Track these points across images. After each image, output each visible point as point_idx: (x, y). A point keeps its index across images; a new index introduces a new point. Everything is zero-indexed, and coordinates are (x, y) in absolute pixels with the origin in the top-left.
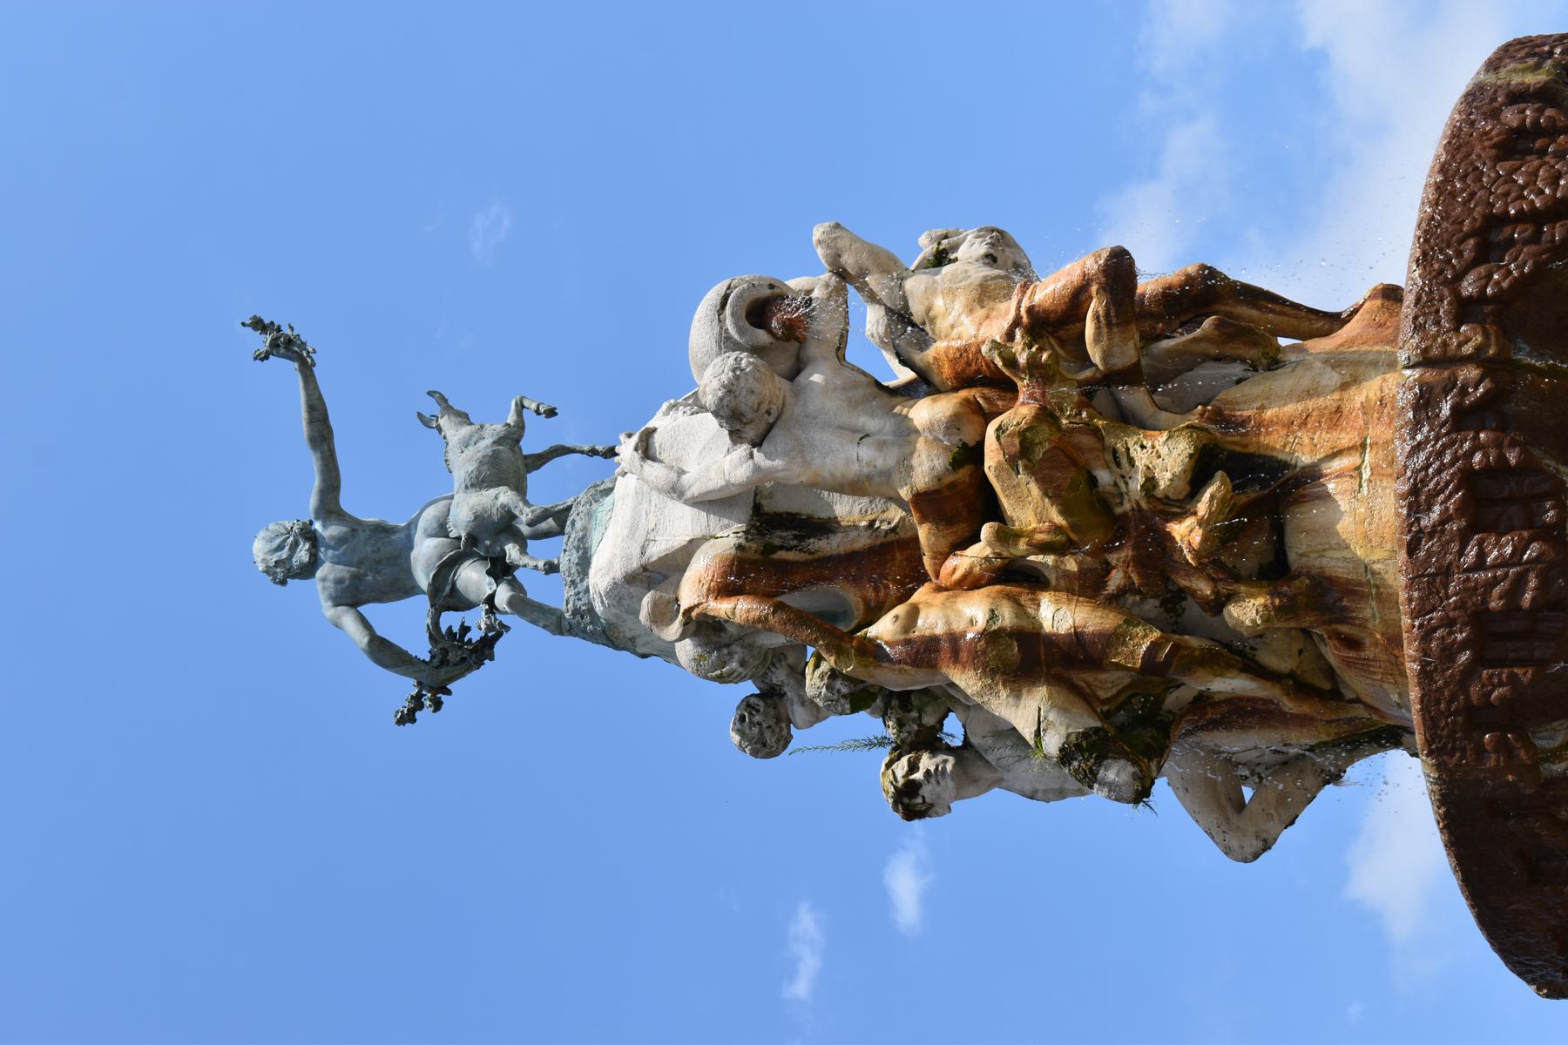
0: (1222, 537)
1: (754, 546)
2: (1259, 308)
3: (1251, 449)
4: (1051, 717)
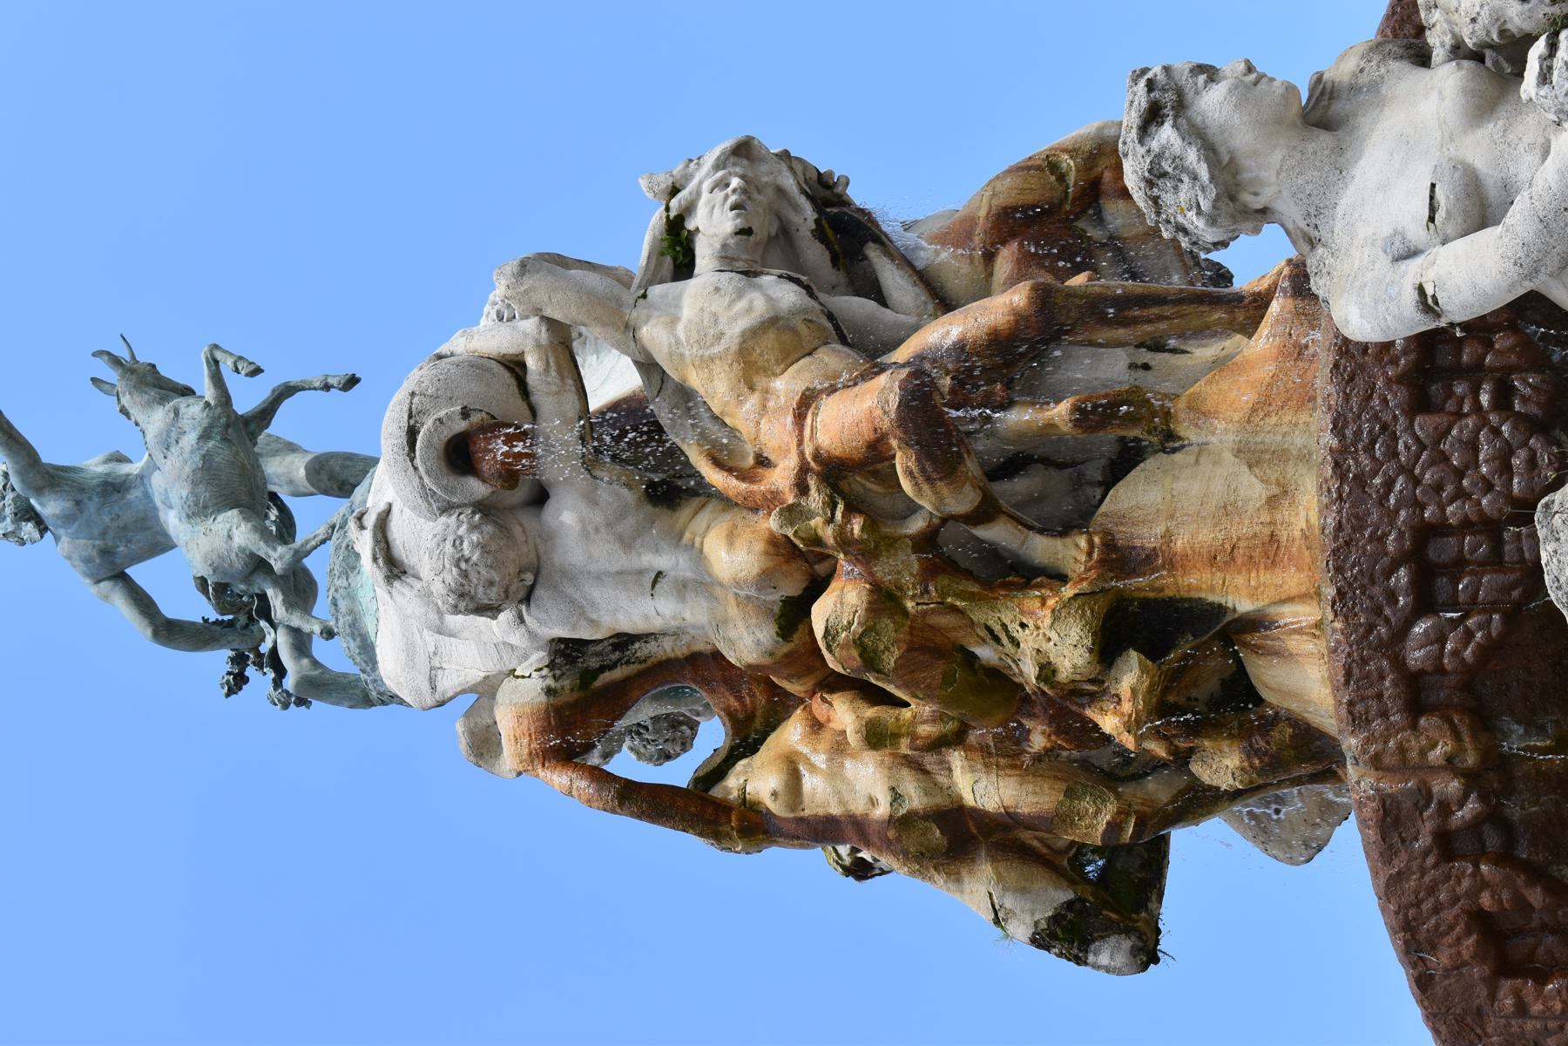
0: (1161, 706)
1: (566, 683)
3: (1169, 593)
4: (1009, 903)
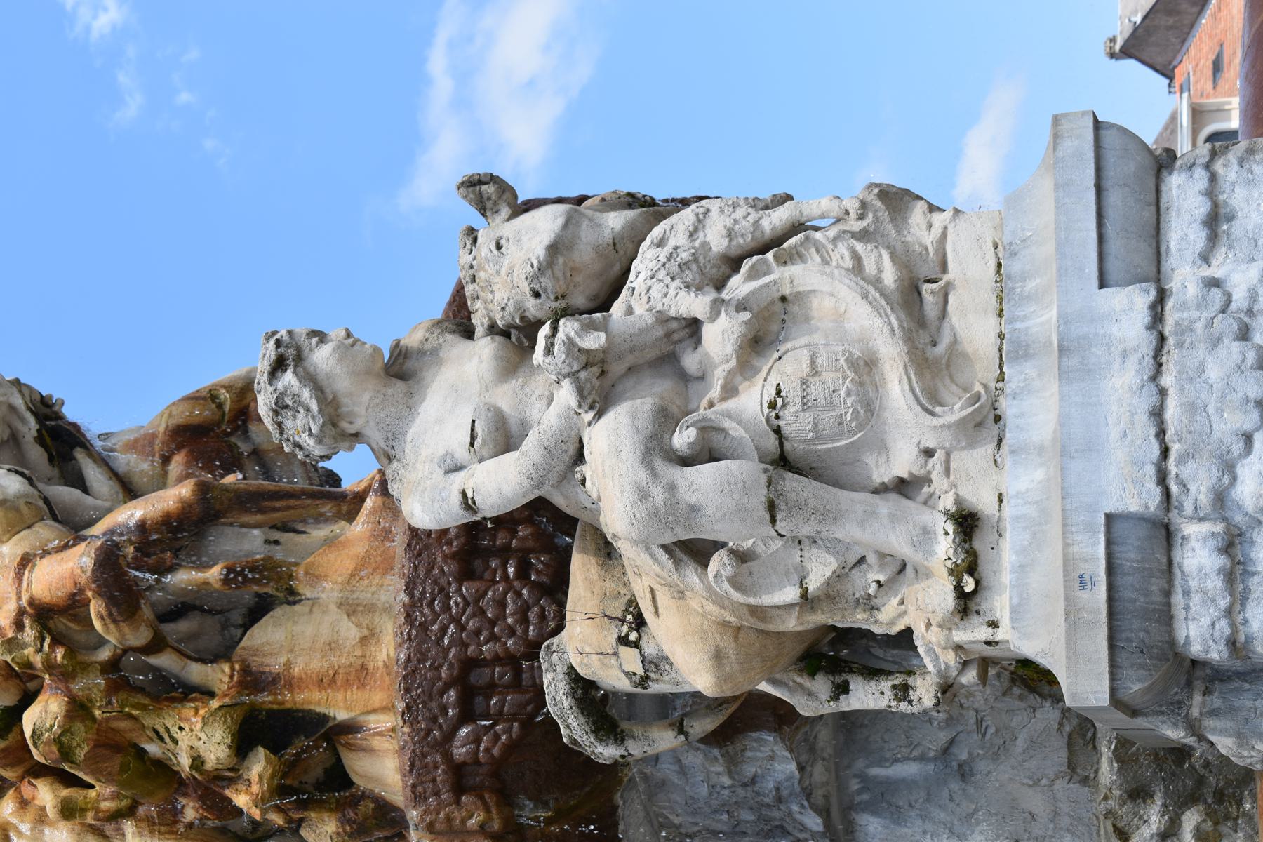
2: (262, 511)
3: (288, 706)
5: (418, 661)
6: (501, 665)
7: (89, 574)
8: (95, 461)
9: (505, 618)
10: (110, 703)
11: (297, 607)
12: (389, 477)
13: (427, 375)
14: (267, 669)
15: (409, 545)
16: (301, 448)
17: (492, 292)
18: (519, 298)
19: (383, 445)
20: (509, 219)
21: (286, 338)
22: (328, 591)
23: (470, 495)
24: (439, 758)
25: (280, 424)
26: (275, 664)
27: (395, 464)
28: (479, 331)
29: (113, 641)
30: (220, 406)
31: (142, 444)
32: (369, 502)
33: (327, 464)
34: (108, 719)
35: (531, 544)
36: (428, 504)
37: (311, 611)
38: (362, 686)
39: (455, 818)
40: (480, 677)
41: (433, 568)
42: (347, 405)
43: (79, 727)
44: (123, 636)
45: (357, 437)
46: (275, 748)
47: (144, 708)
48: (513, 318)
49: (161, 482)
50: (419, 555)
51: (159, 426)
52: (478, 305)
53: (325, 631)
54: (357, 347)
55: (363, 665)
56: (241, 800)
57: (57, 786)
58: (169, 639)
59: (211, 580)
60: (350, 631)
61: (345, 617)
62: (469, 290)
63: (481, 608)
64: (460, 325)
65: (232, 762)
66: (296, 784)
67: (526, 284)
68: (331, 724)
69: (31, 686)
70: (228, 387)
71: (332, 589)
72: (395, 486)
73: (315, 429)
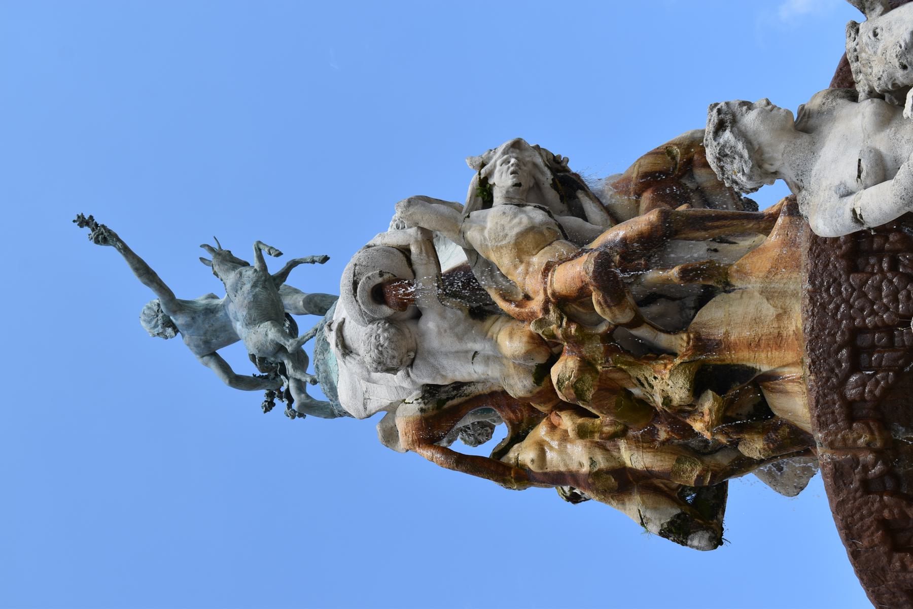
0: (726, 419)
1: (430, 406)
3: (728, 362)
5: (820, 331)
6: (880, 332)
7: (591, 274)
8: (591, 199)
9: (881, 299)
10: (607, 361)
11: (732, 295)
12: (799, 201)
13: (825, 129)
14: (712, 337)
15: (811, 249)
16: (737, 183)
17: (871, 67)
18: (891, 70)
19: (795, 179)
20: (882, 14)
21: (724, 108)
22: (754, 284)
23: (858, 212)
24: (836, 397)
25: (722, 168)
26: (718, 333)
27: (804, 192)
28: (862, 96)
29: (608, 319)
30: (674, 158)
31: (621, 185)
32: (780, 221)
33: (751, 196)
34: (607, 371)
35: (899, 246)
36: (827, 219)
37: (741, 297)
38: (779, 347)
39: (849, 439)
40: (864, 340)
41: (828, 265)
42: (769, 152)
43: (588, 378)
44: (614, 317)
45: (776, 174)
46: (720, 390)
47: (630, 364)
48: (887, 85)
49: (635, 212)
50: (818, 256)
51: (632, 173)
52: (861, 77)
53: (751, 309)
54: (775, 112)
55: (779, 333)
56: (698, 426)
57: (575, 416)
58: (645, 318)
59: (673, 278)
60: (769, 311)
61: (765, 300)
62: (854, 66)
63: (864, 292)
64: (847, 92)
65: (690, 400)
66: (734, 415)
67: (896, 60)
68: (757, 374)
69: (555, 350)
70: (679, 145)
71: (756, 282)
72: (804, 208)
73: (747, 170)
